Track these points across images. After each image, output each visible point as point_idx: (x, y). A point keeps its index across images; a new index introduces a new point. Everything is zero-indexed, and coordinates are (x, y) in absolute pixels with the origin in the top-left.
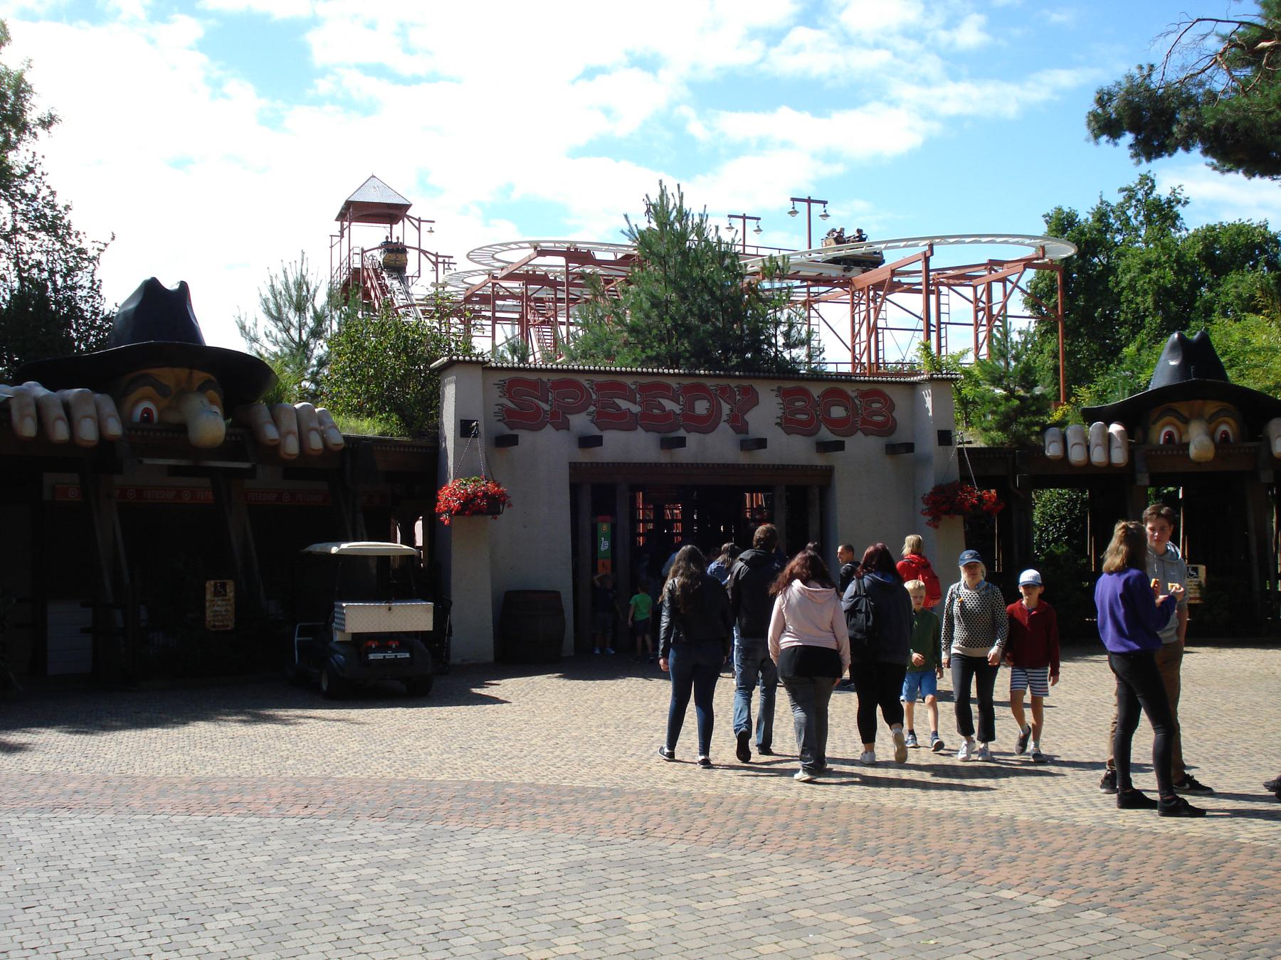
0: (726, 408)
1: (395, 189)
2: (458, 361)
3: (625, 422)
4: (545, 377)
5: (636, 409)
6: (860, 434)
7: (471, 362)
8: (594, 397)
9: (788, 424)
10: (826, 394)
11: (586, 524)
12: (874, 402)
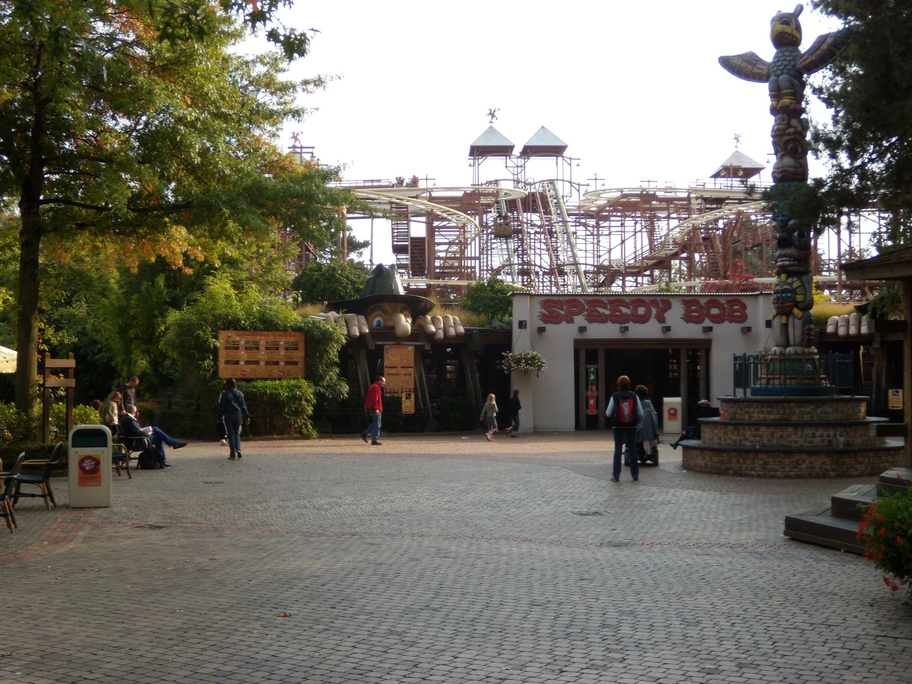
0: (654, 311)
1: (561, 135)
2: (517, 294)
3: (602, 319)
4: (562, 299)
5: (607, 312)
6: (726, 323)
7: (523, 294)
8: (586, 307)
9: (688, 318)
10: (708, 303)
11: (582, 370)
12: (736, 305)
